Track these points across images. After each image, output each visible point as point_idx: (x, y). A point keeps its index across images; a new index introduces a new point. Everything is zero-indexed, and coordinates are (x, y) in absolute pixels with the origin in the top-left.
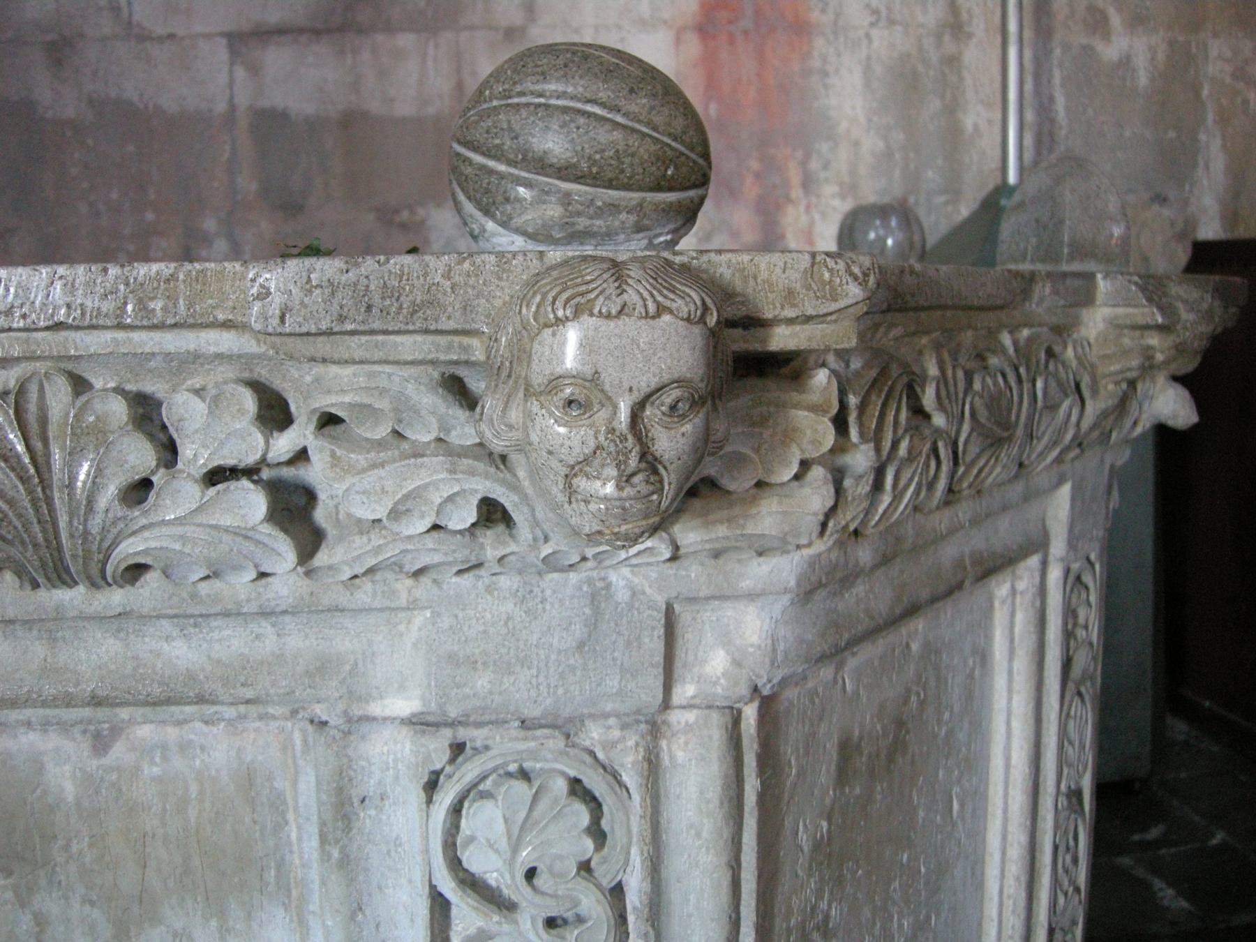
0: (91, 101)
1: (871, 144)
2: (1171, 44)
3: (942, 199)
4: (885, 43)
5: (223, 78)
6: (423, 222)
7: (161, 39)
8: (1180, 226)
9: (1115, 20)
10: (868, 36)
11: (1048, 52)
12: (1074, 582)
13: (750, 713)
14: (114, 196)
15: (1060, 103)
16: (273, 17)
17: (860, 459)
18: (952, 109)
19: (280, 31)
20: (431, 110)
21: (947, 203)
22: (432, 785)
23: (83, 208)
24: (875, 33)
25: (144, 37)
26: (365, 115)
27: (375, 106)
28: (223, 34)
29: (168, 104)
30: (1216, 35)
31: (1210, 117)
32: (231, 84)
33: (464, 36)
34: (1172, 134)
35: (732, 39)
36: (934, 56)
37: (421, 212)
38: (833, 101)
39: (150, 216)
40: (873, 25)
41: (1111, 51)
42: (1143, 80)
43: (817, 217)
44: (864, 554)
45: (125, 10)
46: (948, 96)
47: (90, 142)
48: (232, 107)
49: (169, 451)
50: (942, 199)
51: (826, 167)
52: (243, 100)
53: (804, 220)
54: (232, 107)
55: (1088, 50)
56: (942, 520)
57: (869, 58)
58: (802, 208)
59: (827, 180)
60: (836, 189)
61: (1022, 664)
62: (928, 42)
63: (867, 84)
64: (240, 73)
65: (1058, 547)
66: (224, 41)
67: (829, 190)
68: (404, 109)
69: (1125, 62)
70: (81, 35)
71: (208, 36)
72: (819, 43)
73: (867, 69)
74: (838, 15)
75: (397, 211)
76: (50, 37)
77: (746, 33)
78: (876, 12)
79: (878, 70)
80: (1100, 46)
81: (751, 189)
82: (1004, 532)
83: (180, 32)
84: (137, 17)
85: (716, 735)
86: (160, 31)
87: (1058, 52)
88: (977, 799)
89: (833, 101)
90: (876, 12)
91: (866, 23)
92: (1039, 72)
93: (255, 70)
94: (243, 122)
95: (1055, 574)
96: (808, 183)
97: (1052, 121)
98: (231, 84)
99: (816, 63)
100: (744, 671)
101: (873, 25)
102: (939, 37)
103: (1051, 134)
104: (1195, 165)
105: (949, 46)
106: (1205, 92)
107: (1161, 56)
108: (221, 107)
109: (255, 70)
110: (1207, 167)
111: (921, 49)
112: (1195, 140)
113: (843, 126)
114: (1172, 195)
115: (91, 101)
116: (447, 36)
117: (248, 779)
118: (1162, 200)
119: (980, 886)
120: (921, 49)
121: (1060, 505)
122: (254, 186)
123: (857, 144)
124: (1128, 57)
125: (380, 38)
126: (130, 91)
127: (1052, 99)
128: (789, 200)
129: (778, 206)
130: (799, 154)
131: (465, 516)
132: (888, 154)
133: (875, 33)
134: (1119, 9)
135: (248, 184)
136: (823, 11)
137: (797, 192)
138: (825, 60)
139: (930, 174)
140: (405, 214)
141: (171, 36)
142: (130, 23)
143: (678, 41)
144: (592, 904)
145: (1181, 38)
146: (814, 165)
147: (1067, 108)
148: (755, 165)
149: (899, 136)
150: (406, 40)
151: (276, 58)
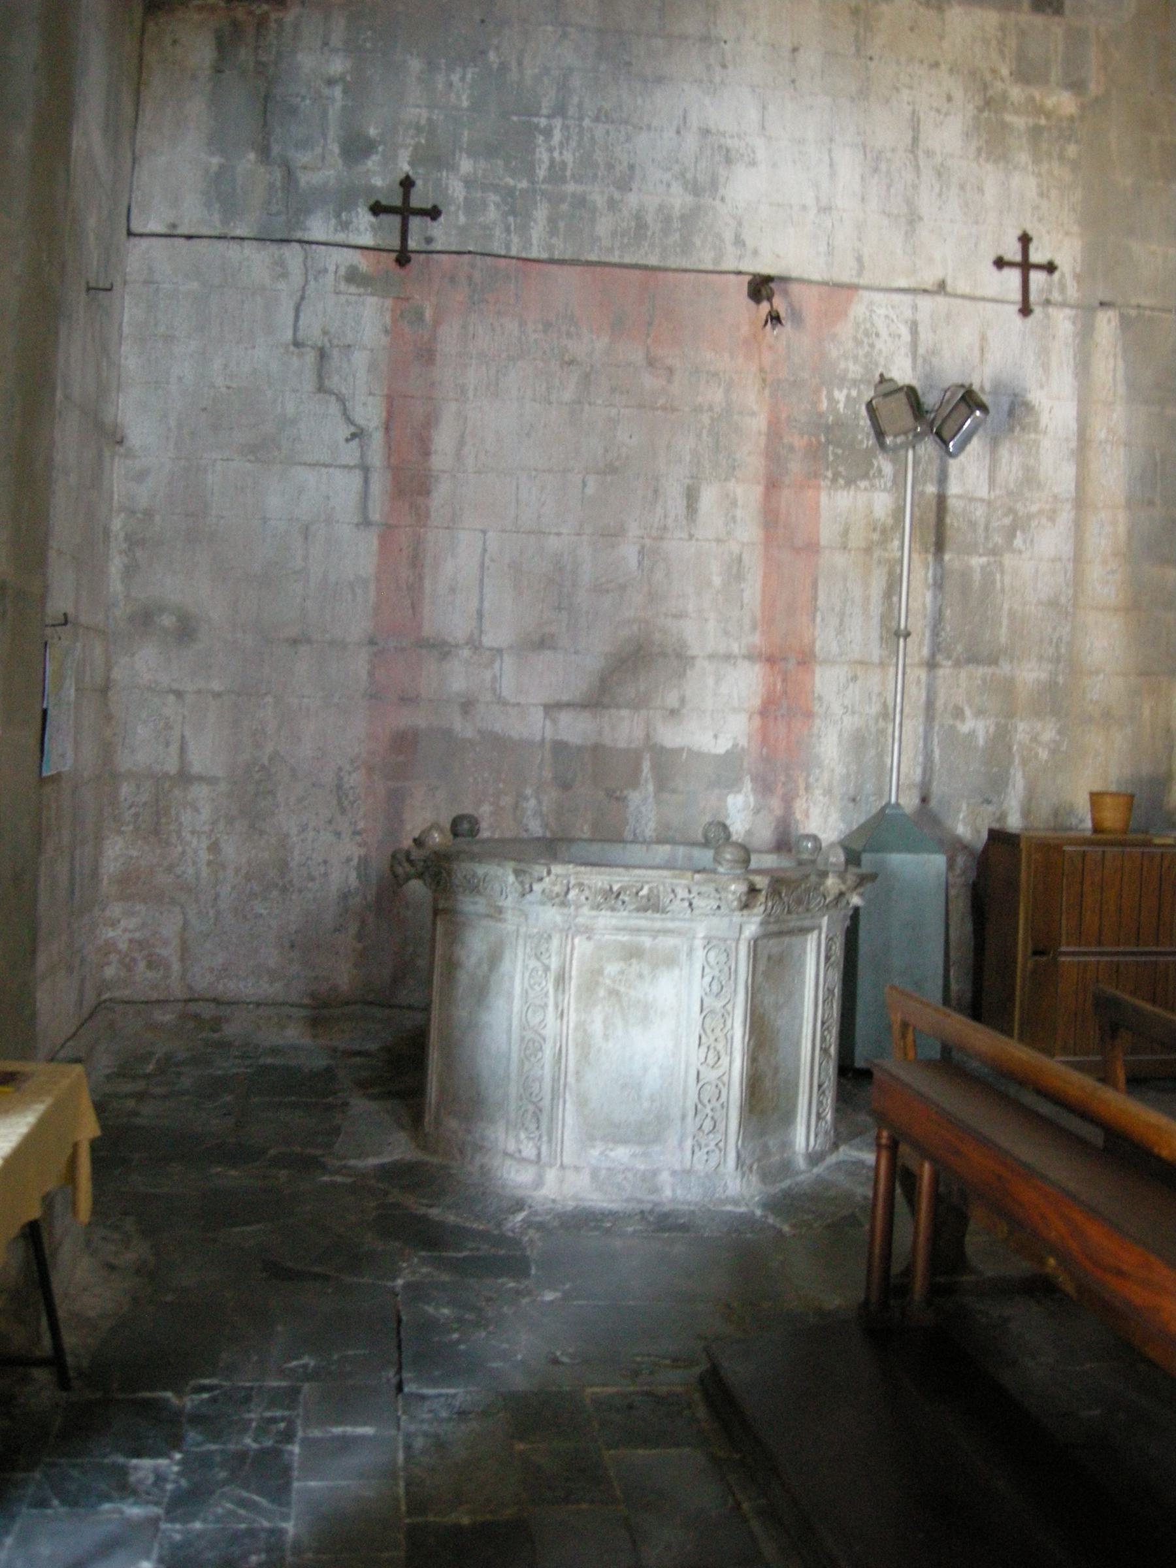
0: (479, 731)
1: (840, 770)
2: (997, 725)
3: (874, 798)
4: (850, 723)
5: (540, 725)
6: (626, 797)
7: (514, 705)
8: (998, 814)
9: (968, 712)
10: (841, 719)
11: (932, 728)
12: (830, 940)
13: (752, 943)
14: (486, 775)
15: (937, 753)
16: (565, 698)
17: (770, 904)
18: (880, 755)
19: (568, 705)
20: (633, 746)
21: (875, 801)
22: (705, 947)
23: (471, 780)
24: (845, 718)
25: (505, 703)
26: (604, 746)
27: (608, 742)
28: (541, 705)
29: (515, 735)
30: (1022, 720)
31: (1017, 760)
32: (544, 727)
33: (651, 712)
34: (995, 769)
35: (776, 718)
36: (873, 730)
37: (625, 792)
38: (823, 749)
39: (501, 785)
40: (844, 713)
41: (965, 728)
42: (981, 742)
43: (811, 805)
44: (772, 920)
45: (498, 691)
46: (880, 749)
47: (478, 749)
48: (543, 739)
49: (676, 896)
50: (874, 798)
51: (817, 780)
52: (549, 734)
53: (805, 806)
54: (543, 739)
55: (952, 727)
56: (789, 917)
57: (841, 730)
58: (804, 800)
59: (817, 787)
60: (821, 791)
61: (814, 954)
62: (871, 723)
63: (840, 741)
64: (548, 723)
65: (824, 929)
66: (542, 708)
67: (818, 792)
68: (622, 744)
69: (972, 734)
70: (478, 701)
71: (535, 705)
72: (818, 722)
73: (840, 735)
74: (828, 708)
75: (614, 792)
76: (463, 700)
77: (782, 716)
78: (846, 707)
79: (846, 735)
80: (958, 724)
81: (780, 791)
82: (807, 923)
83: (523, 701)
84: (504, 694)
85: (746, 944)
86: (513, 701)
87: (936, 728)
88: (803, 982)
89: (823, 749)
90: (846, 707)
91: (841, 712)
92: (927, 738)
93: (555, 722)
94: (548, 746)
95: (823, 936)
96: (808, 788)
97: (932, 762)
98: (544, 727)
99: (815, 730)
100: (687, 409)
101: (844, 713)
102: (877, 721)
103: (931, 769)
104: (1007, 785)
105: (881, 724)
106: (1015, 748)
107: (992, 730)
108: (538, 738)
109: (555, 722)
110: (1014, 786)
111: (867, 726)
112: (1008, 772)
113: (827, 761)
114: (995, 799)
115: (479, 731)
116: (643, 712)
117: (676, 947)
118: (988, 802)
119: (802, 1003)
120: (867, 726)
121: (825, 921)
122: (550, 775)
123: (833, 771)
124: (974, 731)
125: (613, 711)
126: (497, 728)
127: (932, 751)
128: (798, 795)
129: (793, 798)
130: (805, 774)
131: (715, 907)
132: (848, 775)
133: (845, 718)
134: (970, 706)
135: (547, 774)
136: (821, 706)
137: (802, 792)
138: (820, 728)
139: (868, 786)
140: (618, 793)
141: (518, 704)
142: (500, 697)
143: (750, 718)
144: (726, 969)
145: (1003, 722)
146: (811, 780)
147: (940, 756)
148: (783, 778)
149: (854, 767)
150: (625, 713)
151: (565, 717)
